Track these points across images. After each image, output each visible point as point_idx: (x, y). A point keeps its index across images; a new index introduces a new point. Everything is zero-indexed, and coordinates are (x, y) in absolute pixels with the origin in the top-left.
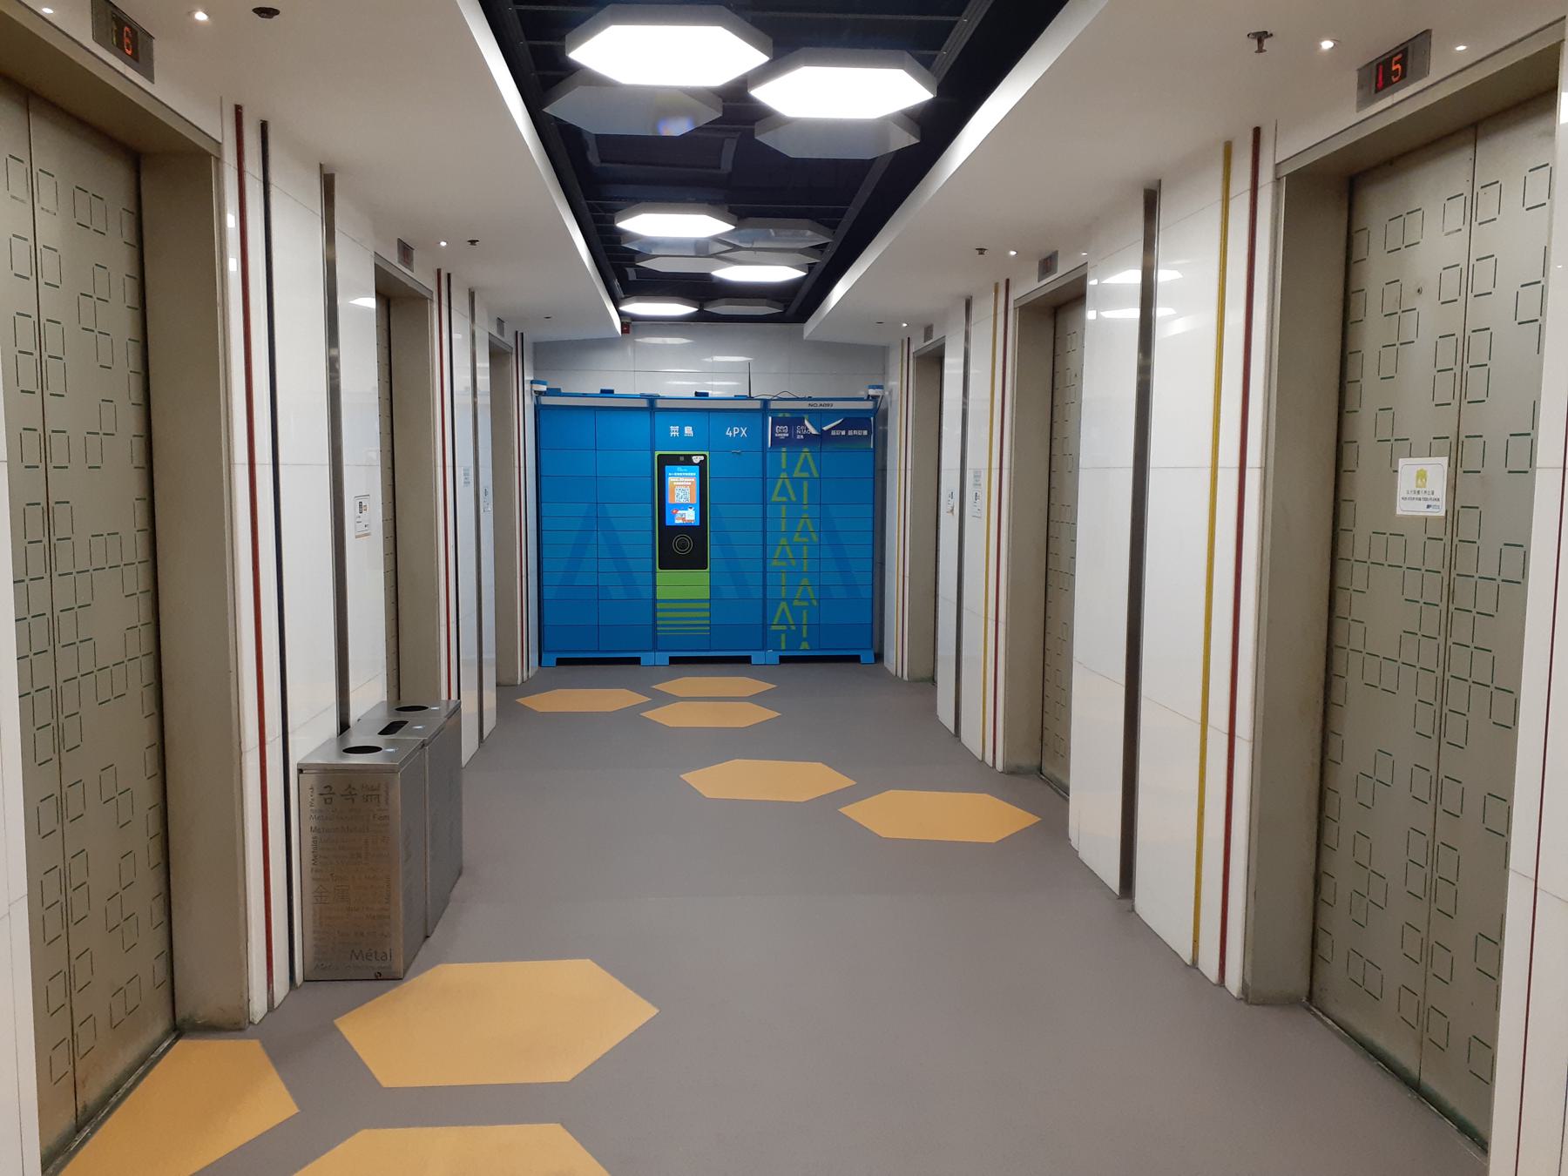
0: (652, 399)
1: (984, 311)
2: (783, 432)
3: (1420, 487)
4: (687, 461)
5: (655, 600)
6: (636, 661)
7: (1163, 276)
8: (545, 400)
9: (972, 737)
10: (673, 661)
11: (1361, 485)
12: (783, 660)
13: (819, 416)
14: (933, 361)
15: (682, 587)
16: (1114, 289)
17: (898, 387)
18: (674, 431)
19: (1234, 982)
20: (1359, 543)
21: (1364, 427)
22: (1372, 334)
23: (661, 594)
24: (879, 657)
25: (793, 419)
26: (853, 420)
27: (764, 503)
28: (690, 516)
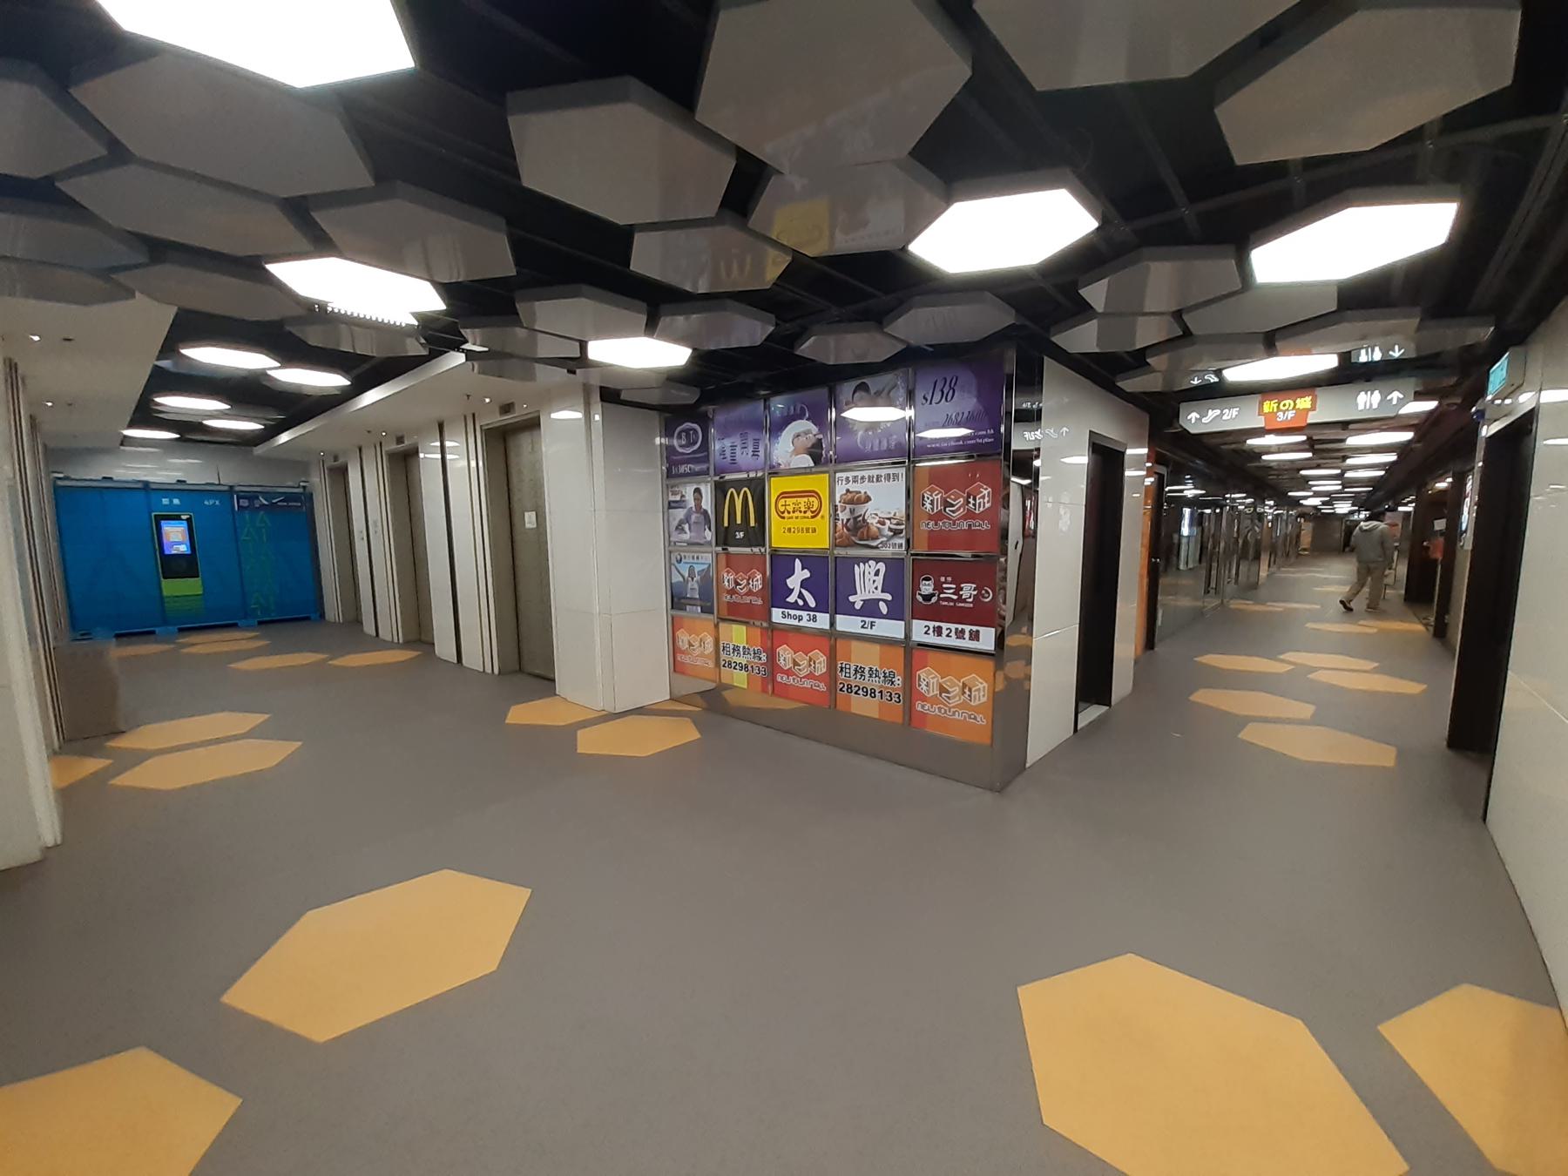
0: (146, 484)
1: (369, 455)
2: (245, 503)
3: (530, 519)
4: (178, 518)
5: (162, 597)
6: (153, 633)
7: (448, 444)
8: (60, 483)
9: (385, 634)
10: (181, 630)
11: (516, 520)
12: (260, 623)
13: (266, 495)
14: (341, 473)
15: (176, 588)
16: (429, 456)
17: (319, 483)
18: (165, 501)
19: (496, 671)
20: (517, 538)
21: (516, 506)
22: (514, 479)
23: (165, 593)
24: (322, 616)
25: (252, 497)
26: (289, 497)
27: (237, 540)
28: (184, 549)
